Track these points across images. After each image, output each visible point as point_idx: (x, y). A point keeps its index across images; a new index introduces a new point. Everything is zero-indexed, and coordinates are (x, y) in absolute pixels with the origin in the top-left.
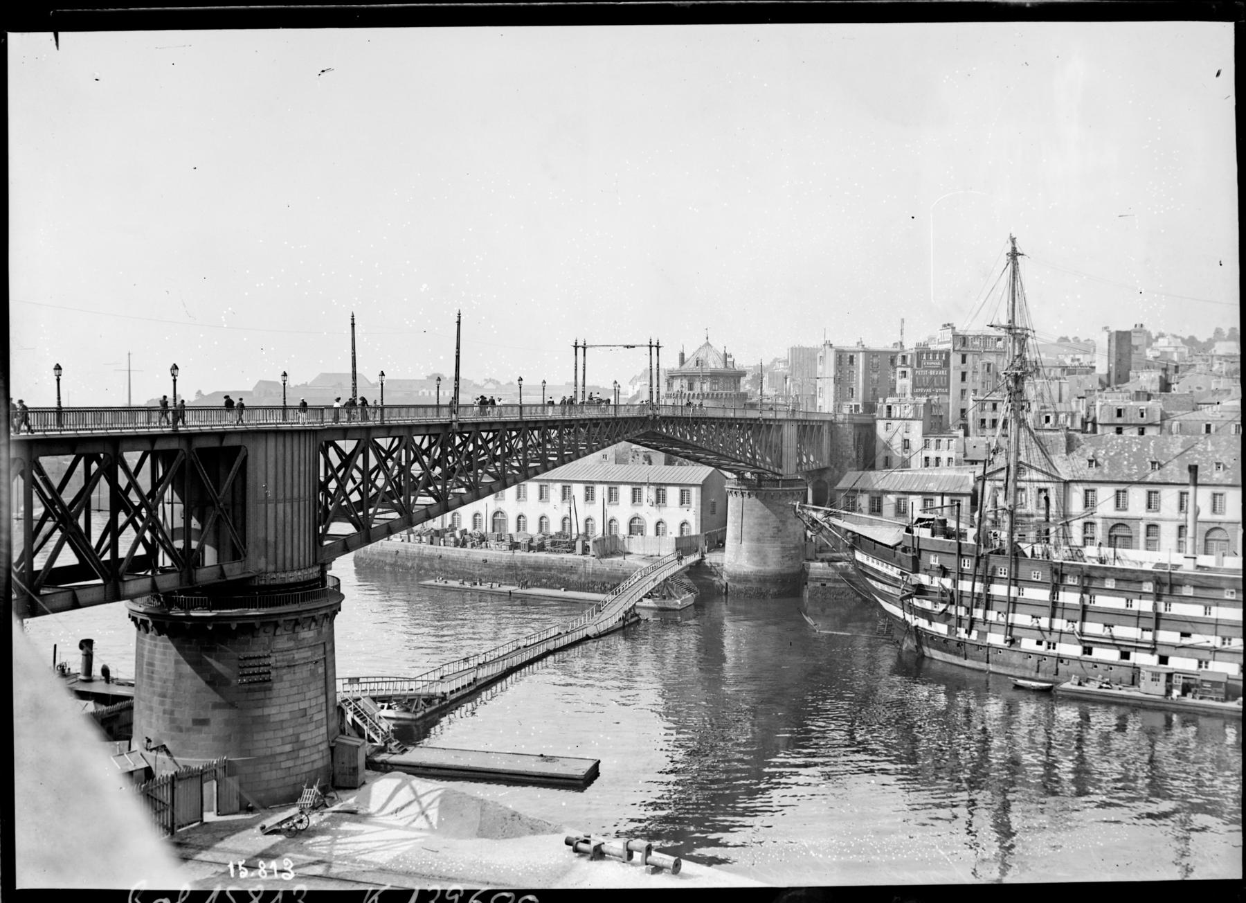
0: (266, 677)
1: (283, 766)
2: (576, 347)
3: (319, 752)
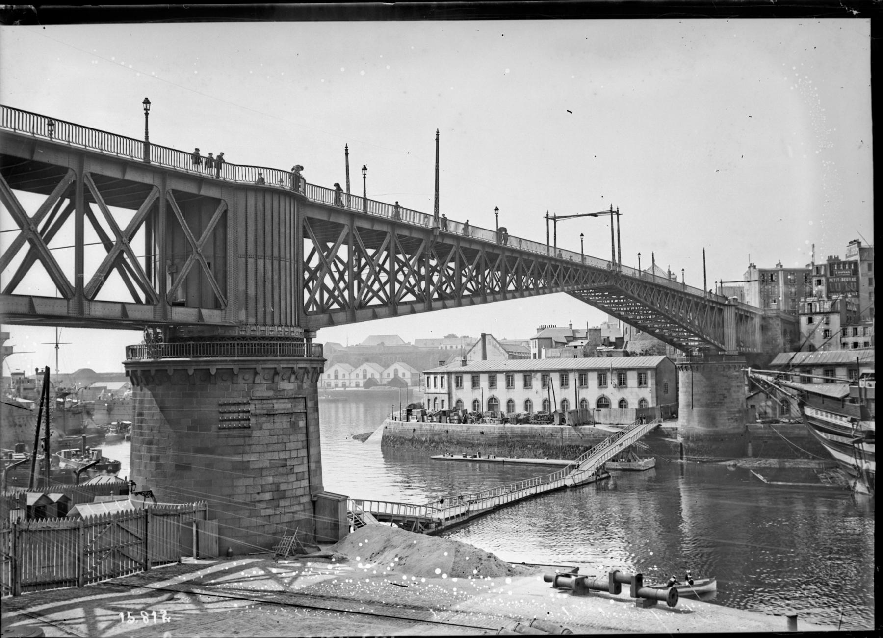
0: (245, 424)
1: (263, 514)
3: (299, 504)
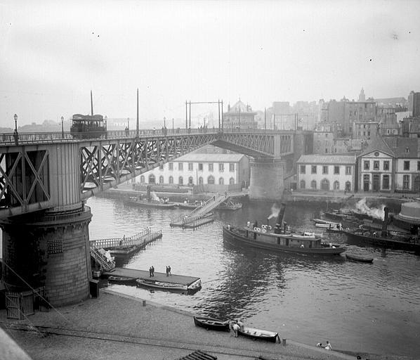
2: (187, 104)
